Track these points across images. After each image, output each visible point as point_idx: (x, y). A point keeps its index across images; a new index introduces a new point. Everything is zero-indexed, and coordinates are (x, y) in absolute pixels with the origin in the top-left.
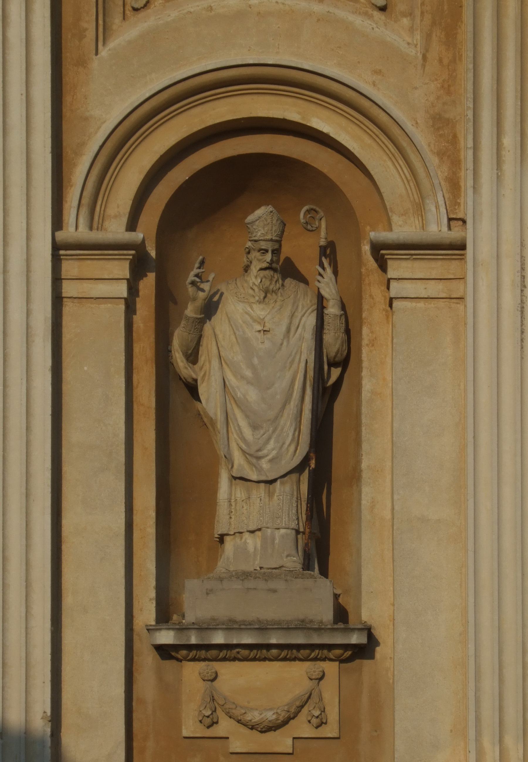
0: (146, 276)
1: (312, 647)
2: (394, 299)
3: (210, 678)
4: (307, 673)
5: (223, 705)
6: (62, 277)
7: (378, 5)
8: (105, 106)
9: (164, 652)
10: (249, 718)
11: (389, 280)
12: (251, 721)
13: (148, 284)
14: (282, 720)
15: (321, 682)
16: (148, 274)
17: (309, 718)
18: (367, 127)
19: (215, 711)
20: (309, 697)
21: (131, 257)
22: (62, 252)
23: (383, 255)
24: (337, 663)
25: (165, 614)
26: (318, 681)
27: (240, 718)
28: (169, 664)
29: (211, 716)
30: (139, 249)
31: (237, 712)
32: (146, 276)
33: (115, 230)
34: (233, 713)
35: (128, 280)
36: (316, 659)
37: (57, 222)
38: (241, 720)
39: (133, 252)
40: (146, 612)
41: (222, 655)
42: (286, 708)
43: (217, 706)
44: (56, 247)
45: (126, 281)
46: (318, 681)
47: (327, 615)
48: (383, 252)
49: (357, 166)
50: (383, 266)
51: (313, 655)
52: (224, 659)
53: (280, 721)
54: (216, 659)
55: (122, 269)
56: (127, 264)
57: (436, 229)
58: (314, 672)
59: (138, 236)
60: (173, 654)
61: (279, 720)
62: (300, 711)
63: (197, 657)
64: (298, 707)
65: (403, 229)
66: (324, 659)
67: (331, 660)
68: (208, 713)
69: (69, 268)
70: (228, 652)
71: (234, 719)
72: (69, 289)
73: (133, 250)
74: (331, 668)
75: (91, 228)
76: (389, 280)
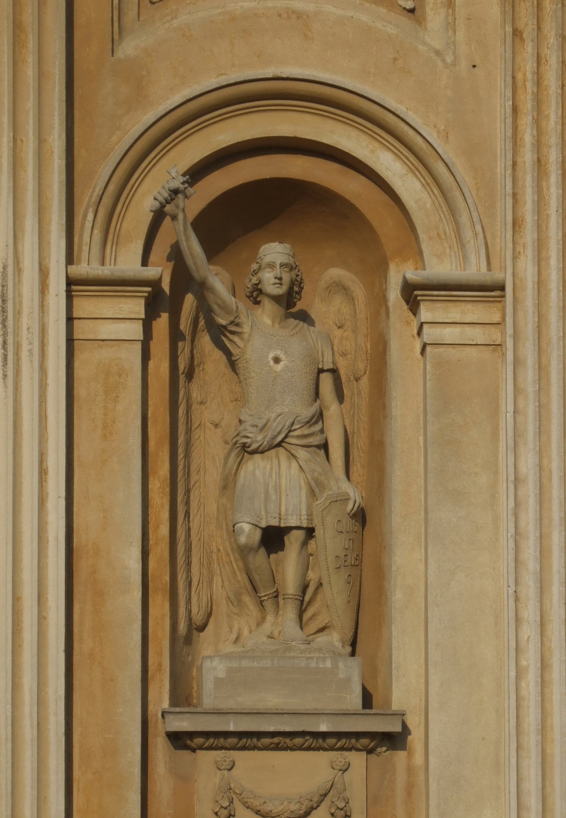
0: (160, 316)
1: (339, 735)
2: (427, 346)
3: (227, 767)
4: (332, 762)
5: (240, 794)
6: (74, 316)
7: (408, 7)
8: (117, 132)
9: (178, 739)
10: (270, 809)
11: (422, 324)
12: (271, 811)
13: (162, 323)
14: (305, 810)
15: (346, 773)
16: (161, 314)
17: (333, 811)
18: (393, 146)
19: (232, 802)
20: (332, 786)
21: (146, 294)
22: (74, 288)
23: (417, 296)
24: (365, 752)
25: (182, 696)
26: (342, 772)
27: (258, 808)
28: (185, 754)
29: (228, 808)
30: (155, 284)
31: (256, 803)
32: (160, 316)
33: (128, 261)
34: (251, 803)
35: (142, 341)
36: (342, 749)
37: (70, 259)
38: (259, 811)
39: (149, 289)
40: (161, 698)
41: (241, 743)
42: (309, 797)
43: (234, 796)
44: (70, 282)
45: (141, 321)
46: (342, 772)
47: (355, 700)
48: (416, 293)
49: (384, 191)
50: (413, 305)
51: (339, 744)
52: (244, 748)
53: (302, 812)
54: (234, 748)
55: (136, 307)
56: (142, 302)
57: (475, 270)
58: (340, 762)
59: (151, 272)
60: (189, 742)
61: (301, 810)
62: (322, 801)
63: (214, 745)
64: (321, 795)
65: (440, 266)
66: (349, 749)
67: (358, 750)
68: (226, 804)
69: (83, 307)
70: (248, 740)
71: (252, 809)
72: (81, 330)
73: (149, 286)
74: (357, 760)
75: (103, 263)
76: (422, 324)
